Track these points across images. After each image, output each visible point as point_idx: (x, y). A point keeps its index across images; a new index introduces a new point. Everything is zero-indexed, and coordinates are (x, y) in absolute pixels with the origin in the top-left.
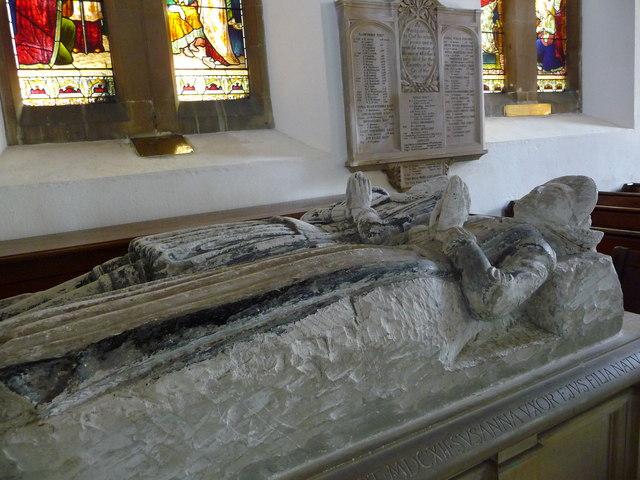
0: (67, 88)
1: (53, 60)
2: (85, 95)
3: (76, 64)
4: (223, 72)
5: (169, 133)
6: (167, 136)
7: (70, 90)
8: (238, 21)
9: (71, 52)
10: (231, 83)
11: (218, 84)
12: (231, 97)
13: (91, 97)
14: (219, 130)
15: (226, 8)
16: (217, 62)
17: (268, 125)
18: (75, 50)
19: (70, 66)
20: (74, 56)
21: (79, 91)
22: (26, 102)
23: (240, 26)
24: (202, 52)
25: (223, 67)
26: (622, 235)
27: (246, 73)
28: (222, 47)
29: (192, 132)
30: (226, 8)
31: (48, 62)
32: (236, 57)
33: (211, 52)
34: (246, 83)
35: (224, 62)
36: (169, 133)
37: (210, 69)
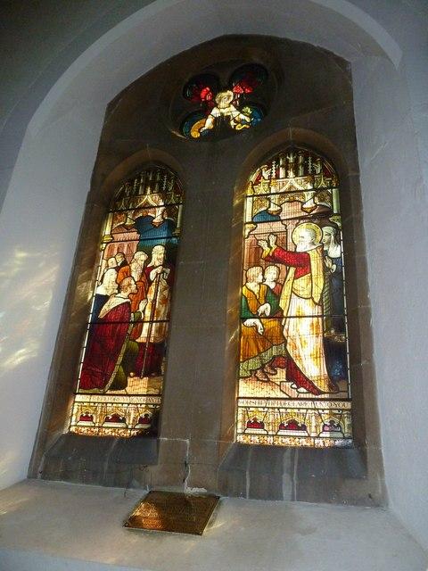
0: (289, 423)
1: (109, 385)
2: (128, 429)
3: (129, 390)
4: (309, 404)
5: (203, 490)
6: (200, 493)
7: (293, 425)
8: (340, 329)
9: (128, 375)
10: (318, 425)
11: (300, 420)
12: (319, 443)
13: (318, 437)
14: (280, 497)
15: (322, 316)
16: (302, 390)
17: (375, 501)
18: (132, 374)
19: (122, 392)
20: (129, 380)
21: (304, 428)
22: (240, 439)
23: (344, 338)
24: (281, 375)
25: (311, 396)
26: (182, 217)
27: (348, 405)
28: (313, 368)
29: (238, 493)
30: (322, 316)
31: (104, 387)
32: (333, 381)
33: (295, 375)
34: (347, 422)
35: (312, 389)
36: (203, 490)
37: (290, 399)
